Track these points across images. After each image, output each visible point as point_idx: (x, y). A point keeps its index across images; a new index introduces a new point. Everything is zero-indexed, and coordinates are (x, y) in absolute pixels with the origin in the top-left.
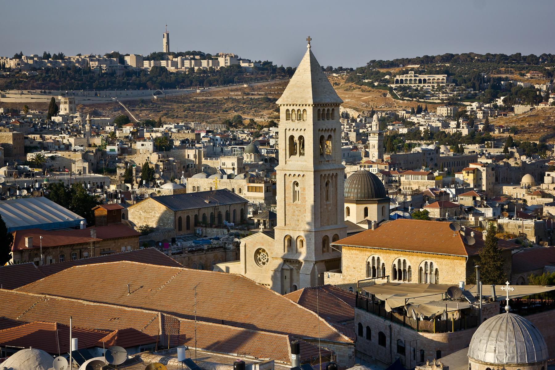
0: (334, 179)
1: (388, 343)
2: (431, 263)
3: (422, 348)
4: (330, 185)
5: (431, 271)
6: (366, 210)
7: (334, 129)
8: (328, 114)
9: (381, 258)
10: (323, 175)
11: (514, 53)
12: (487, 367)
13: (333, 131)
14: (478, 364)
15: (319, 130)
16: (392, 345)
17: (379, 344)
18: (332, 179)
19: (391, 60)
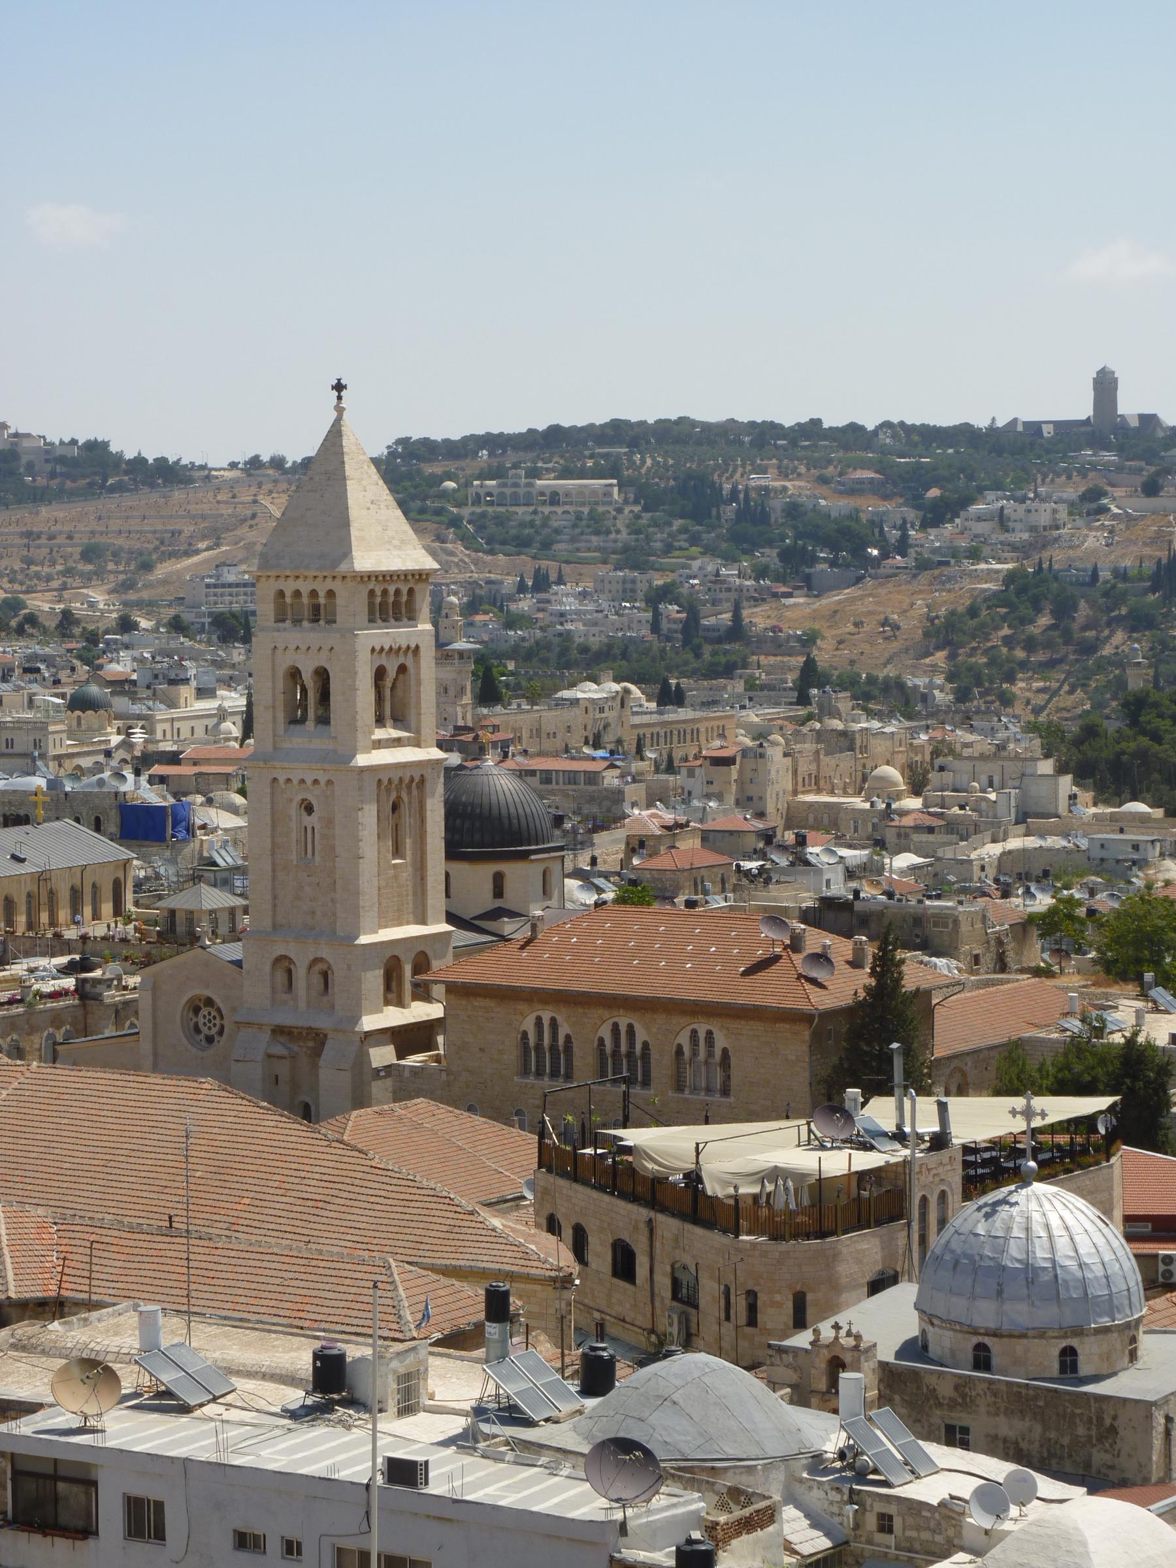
0: (415, 792)
1: (642, 1271)
2: (630, 1028)
3: (750, 1286)
4: (405, 809)
5: (710, 1054)
6: (498, 879)
7: (413, 646)
8: (396, 604)
9: (559, 1019)
10: (385, 782)
11: (804, 419)
12: (975, 1340)
13: (410, 654)
14: (951, 1333)
15: (373, 650)
16: (657, 1277)
17: (615, 1274)
18: (409, 793)
19: (456, 436)
